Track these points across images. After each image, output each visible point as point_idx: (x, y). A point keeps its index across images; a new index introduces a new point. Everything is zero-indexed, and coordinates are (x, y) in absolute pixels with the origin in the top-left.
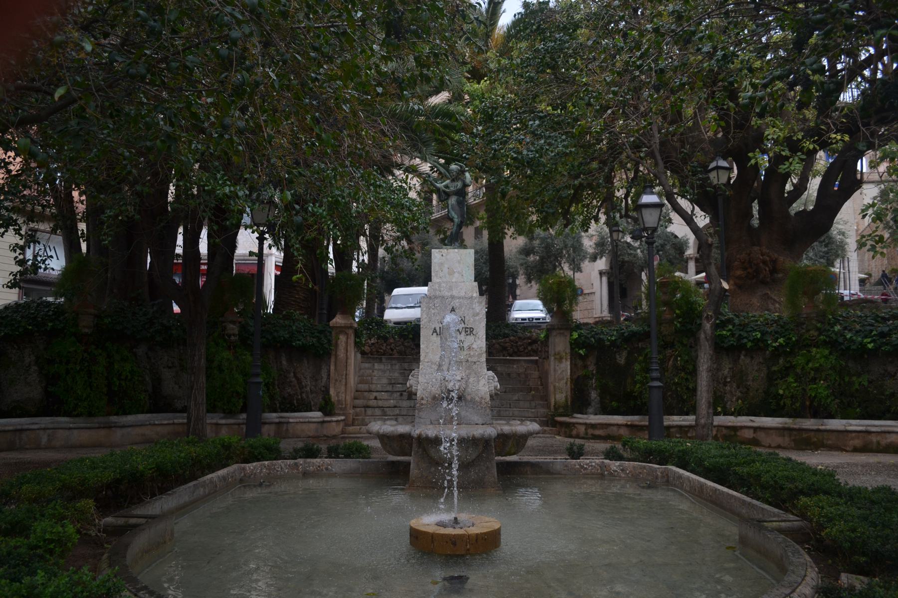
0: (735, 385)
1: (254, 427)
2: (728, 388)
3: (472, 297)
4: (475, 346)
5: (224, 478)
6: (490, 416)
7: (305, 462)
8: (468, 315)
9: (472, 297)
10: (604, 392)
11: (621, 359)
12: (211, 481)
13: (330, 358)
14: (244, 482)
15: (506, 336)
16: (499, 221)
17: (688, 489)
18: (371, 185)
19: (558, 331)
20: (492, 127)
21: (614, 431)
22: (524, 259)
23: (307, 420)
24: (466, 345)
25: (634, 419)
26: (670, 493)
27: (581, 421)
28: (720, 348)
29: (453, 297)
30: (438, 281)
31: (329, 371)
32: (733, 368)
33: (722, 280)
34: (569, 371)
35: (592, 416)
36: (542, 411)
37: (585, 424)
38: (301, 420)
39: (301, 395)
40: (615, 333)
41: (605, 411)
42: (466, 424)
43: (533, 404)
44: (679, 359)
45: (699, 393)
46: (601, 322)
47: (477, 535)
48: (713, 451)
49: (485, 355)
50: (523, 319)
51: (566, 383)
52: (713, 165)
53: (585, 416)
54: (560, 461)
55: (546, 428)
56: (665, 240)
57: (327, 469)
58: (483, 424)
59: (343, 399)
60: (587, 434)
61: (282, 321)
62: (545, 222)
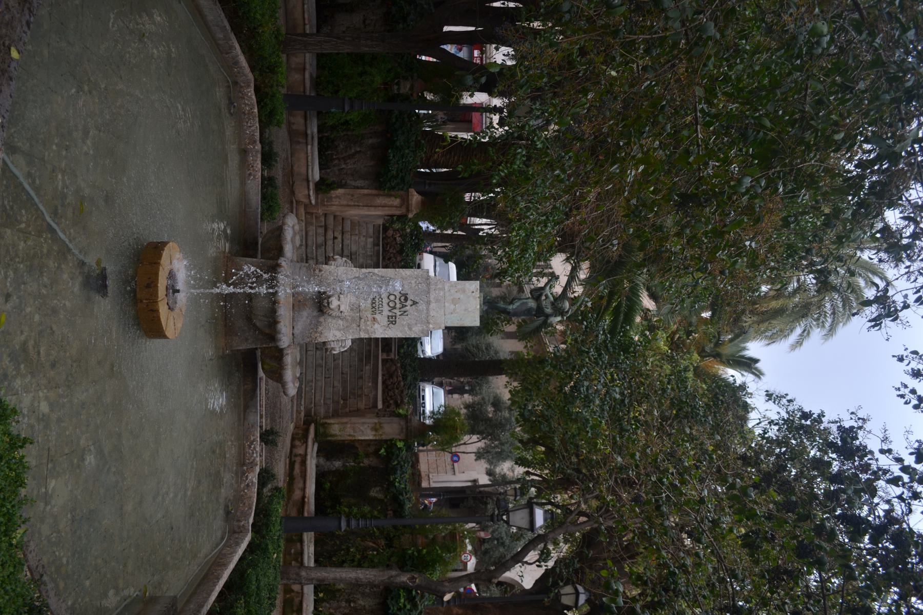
0: (347, 611)
1: (296, 101)
2: (344, 604)
3: (429, 323)
4: (376, 326)
5: (236, 63)
6: (302, 342)
7: (257, 152)
8: (410, 319)
9: (429, 323)
10: (341, 474)
11: (375, 492)
12: (232, 47)
13: (376, 189)
14: (234, 85)
15: (405, 377)
16: (524, 370)
17: (224, 552)
18: (547, 217)
19: (404, 427)
20: (614, 352)
21: (298, 484)
22: (489, 400)
23: (310, 164)
24: (378, 317)
25: (311, 507)
26: (219, 534)
27: (309, 450)
28: (387, 592)
29: (428, 303)
30: (446, 288)
31: (362, 188)
32: (365, 609)
33: (453, 593)
34: (363, 438)
35: (314, 462)
36: (322, 411)
37: (306, 455)
38: (310, 158)
39: (336, 159)
40: (403, 486)
41: (321, 476)
42: (293, 316)
43: (329, 402)
44: (375, 553)
45: (334, 569)
46: (416, 477)
47: (157, 311)
48: (266, 580)
49: (367, 336)
50: (423, 397)
51: (350, 435)
52: (581, 589)
53: (315, 455)
54: (259, 420)
55: (303, 414)
56: (509, 546)
57: (250, 174)
58: (293, 334)
59: (333, 203)
60: (296, 456)
61: (414, 138)
62: (524, 419)
